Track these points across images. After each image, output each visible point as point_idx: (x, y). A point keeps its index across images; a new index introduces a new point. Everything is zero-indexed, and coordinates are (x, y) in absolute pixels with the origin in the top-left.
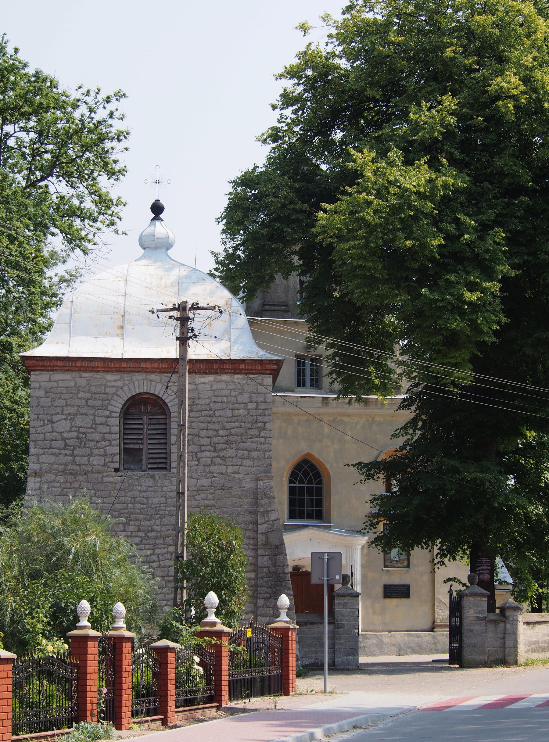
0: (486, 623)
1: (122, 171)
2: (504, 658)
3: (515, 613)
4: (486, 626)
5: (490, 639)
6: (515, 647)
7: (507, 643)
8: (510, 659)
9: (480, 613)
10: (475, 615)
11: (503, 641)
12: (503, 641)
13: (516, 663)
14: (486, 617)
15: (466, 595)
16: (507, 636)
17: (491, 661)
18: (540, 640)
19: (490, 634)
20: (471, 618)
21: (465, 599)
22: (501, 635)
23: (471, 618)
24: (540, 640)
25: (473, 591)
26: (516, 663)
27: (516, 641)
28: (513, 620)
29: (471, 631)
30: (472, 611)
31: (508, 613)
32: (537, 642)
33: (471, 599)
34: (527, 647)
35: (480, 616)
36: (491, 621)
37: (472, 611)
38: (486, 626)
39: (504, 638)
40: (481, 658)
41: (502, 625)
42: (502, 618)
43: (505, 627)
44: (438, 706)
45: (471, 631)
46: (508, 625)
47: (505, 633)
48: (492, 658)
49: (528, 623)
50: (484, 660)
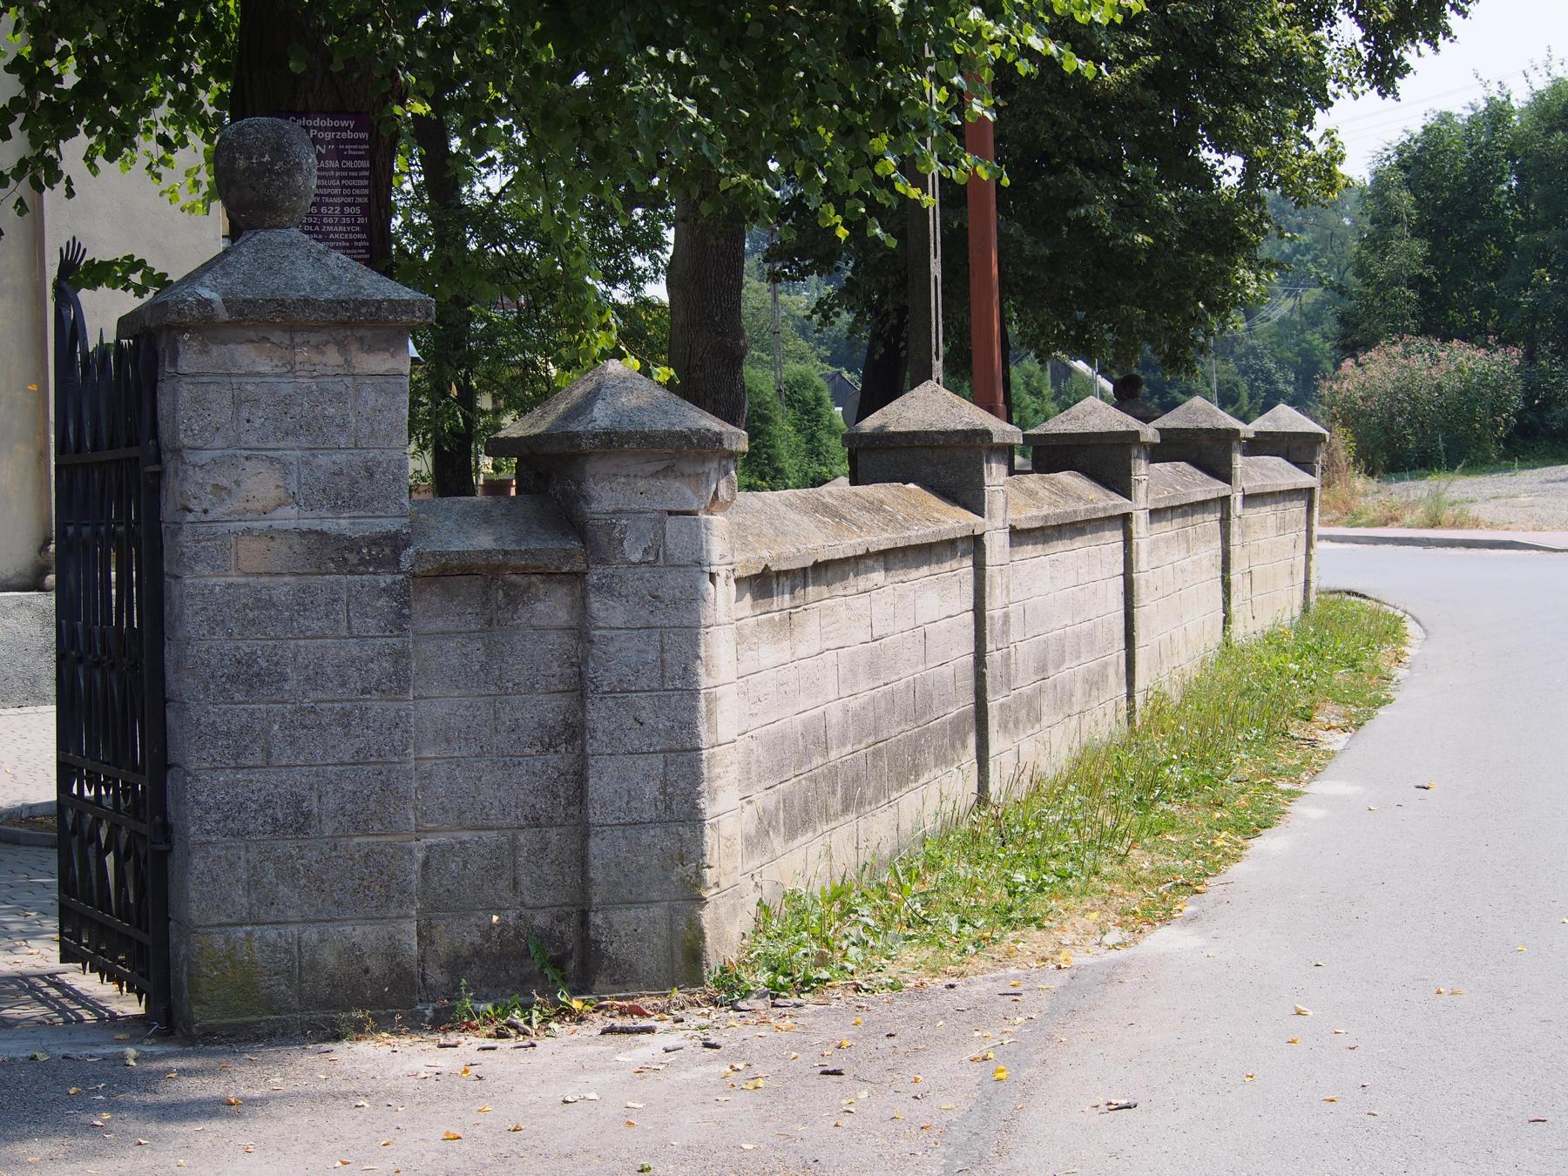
0: (402, 598)
1: (8, 69)
2: (579, 933)
3: (679, 492)
4: (399, 621)
5: (440, 745)
6: (682, 813)
7: (600, 786)
8: (627, 929)
9: (339, 502)
10: (289, 518)
11: (560, 759)
12: (560, 759)
13: (685, 966)
14: (397, 542)
15: (206, 326)
16: (598, 715)
17: (456, 965)
18: (835, 714)
19: (438, 705)
20: (252, 553)
21: (190, 359)
22: (548, 708)
23: (252, 553)
24: (835, 714)
25: (272, 285)
26: (685, 966)
27: (683, 760)
28: (658, 557)
29: (252, 677)
30: (261, 485)
31: (607, 494)
32: (817, 738)
33: (252, 359)
34: (764, 799)
35: (341, 524)
36: (451, 573)
37: (261, 485)
38: (399, 621)
39: (574, 732)
40: (363, 934)
41: (552, 607)
42: (549, 546)
43: (581, 631)
44: (272, 1053)
45: (252, 677)
46: (609, 613)
47: (579, 687)
48: (459, 934)
49: (762, 583)
50: (392, 953)
